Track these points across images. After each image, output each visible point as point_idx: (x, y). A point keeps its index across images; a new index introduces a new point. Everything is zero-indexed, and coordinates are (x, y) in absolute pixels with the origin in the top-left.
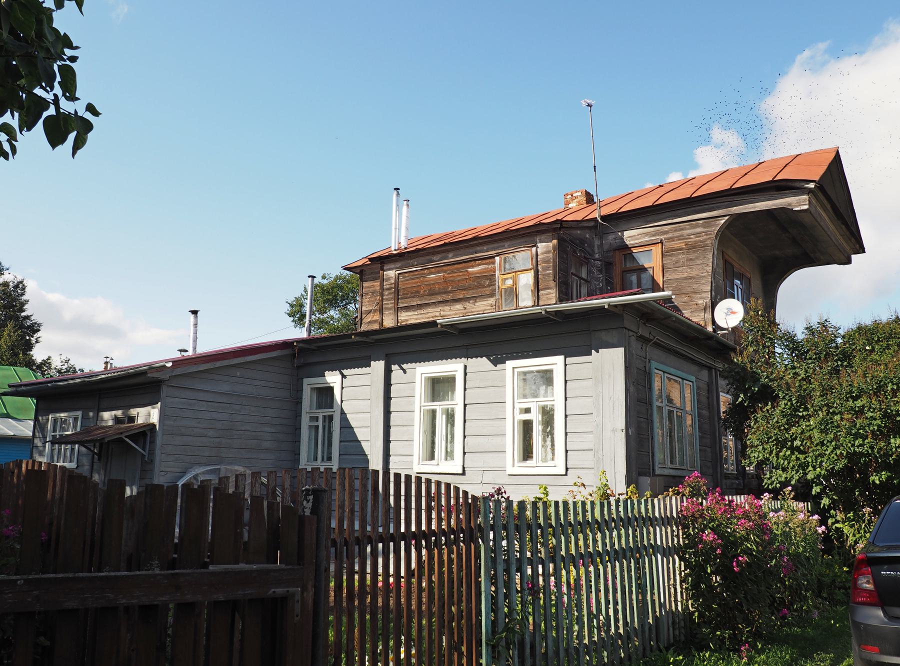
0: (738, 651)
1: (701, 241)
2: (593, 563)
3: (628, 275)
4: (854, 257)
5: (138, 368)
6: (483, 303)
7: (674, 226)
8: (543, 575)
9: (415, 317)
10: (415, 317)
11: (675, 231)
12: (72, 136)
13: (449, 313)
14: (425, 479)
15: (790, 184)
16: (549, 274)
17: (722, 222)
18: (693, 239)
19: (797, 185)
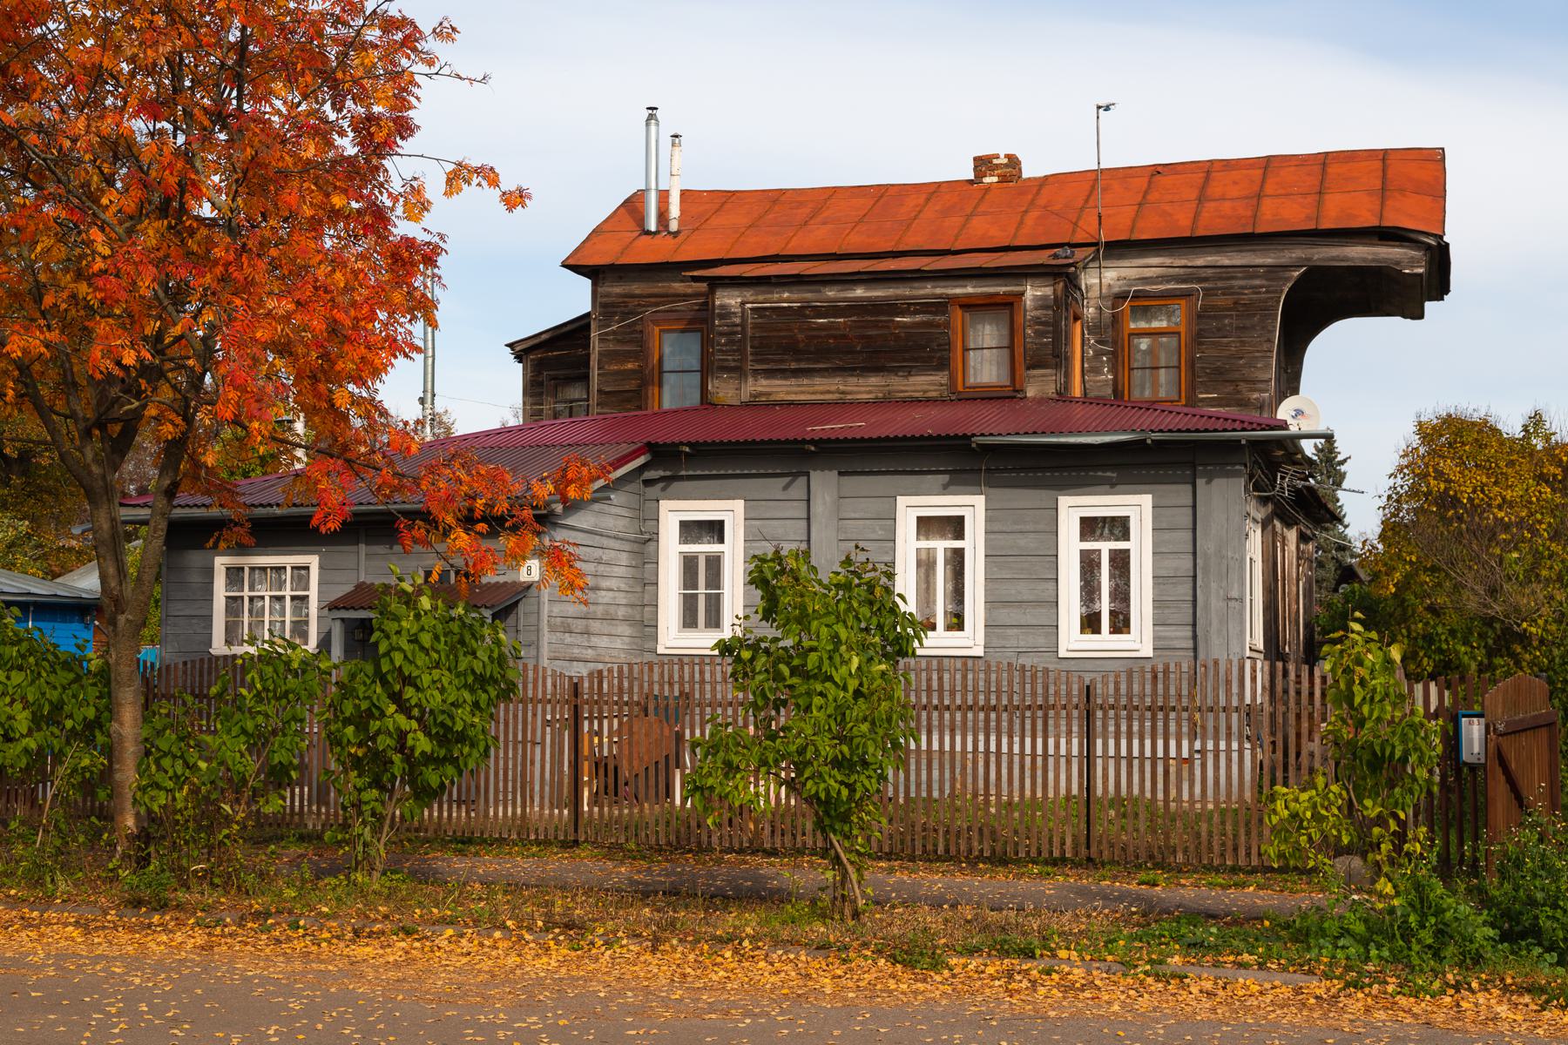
0: (1557, 443)
1: (1260, 301)
2: (669, 843)
3: (1136, 341)
4: (1429, 306)
5: (964, 471)
6: (923, 378)
7: (1218, 270)
8: (990, 692)
9: (784, 389)
10: (784, 389)
11: (1221, 279)
12: (675, 210)
13: (855, 389)
14: (1128, 551)
15: (1403, 233)
16: (1046, 344)
17: (1296, 274)
18: (1248, 296)
19: (1413, 236)
